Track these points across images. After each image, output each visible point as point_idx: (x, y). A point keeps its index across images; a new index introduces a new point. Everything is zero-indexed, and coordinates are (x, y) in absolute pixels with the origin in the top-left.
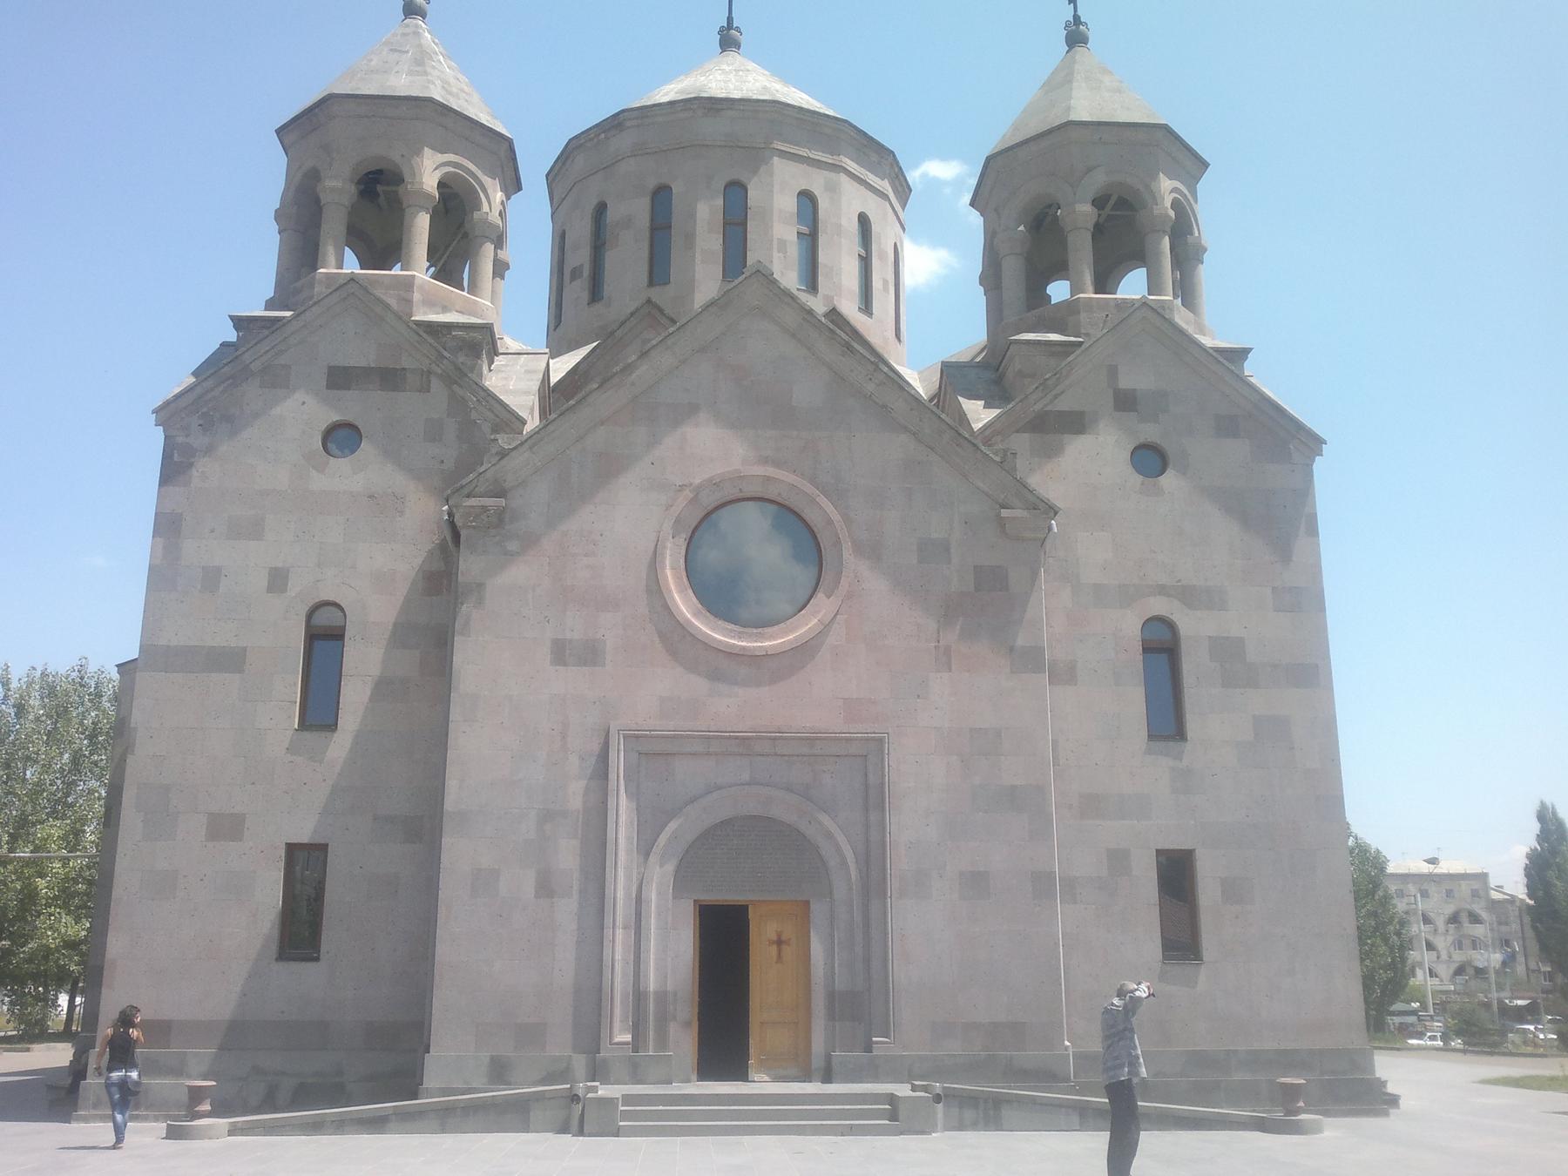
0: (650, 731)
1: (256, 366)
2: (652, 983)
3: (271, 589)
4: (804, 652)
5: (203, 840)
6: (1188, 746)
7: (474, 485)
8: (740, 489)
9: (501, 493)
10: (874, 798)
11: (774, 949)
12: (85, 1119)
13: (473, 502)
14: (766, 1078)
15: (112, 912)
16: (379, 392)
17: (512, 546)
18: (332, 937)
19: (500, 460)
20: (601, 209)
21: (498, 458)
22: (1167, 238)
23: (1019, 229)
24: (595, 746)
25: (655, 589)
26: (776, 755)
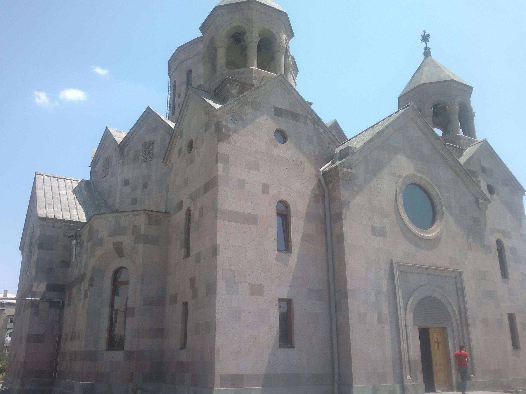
1: (250, 100)
2: (412, 357)
4: (437, 240)
6: (292, 254)
7: (345, 164)
8: (415, 180)
10: (460, 292)
11: (436, 344)
13: (345, 170)
14: (440, 391)
15: (420, 352)
16: (291, 120)
17: (356, 189)
18: (298, 338)
20: (190, 72)
22: (283, 56)
24: (388, 268)
26: (435, 275)
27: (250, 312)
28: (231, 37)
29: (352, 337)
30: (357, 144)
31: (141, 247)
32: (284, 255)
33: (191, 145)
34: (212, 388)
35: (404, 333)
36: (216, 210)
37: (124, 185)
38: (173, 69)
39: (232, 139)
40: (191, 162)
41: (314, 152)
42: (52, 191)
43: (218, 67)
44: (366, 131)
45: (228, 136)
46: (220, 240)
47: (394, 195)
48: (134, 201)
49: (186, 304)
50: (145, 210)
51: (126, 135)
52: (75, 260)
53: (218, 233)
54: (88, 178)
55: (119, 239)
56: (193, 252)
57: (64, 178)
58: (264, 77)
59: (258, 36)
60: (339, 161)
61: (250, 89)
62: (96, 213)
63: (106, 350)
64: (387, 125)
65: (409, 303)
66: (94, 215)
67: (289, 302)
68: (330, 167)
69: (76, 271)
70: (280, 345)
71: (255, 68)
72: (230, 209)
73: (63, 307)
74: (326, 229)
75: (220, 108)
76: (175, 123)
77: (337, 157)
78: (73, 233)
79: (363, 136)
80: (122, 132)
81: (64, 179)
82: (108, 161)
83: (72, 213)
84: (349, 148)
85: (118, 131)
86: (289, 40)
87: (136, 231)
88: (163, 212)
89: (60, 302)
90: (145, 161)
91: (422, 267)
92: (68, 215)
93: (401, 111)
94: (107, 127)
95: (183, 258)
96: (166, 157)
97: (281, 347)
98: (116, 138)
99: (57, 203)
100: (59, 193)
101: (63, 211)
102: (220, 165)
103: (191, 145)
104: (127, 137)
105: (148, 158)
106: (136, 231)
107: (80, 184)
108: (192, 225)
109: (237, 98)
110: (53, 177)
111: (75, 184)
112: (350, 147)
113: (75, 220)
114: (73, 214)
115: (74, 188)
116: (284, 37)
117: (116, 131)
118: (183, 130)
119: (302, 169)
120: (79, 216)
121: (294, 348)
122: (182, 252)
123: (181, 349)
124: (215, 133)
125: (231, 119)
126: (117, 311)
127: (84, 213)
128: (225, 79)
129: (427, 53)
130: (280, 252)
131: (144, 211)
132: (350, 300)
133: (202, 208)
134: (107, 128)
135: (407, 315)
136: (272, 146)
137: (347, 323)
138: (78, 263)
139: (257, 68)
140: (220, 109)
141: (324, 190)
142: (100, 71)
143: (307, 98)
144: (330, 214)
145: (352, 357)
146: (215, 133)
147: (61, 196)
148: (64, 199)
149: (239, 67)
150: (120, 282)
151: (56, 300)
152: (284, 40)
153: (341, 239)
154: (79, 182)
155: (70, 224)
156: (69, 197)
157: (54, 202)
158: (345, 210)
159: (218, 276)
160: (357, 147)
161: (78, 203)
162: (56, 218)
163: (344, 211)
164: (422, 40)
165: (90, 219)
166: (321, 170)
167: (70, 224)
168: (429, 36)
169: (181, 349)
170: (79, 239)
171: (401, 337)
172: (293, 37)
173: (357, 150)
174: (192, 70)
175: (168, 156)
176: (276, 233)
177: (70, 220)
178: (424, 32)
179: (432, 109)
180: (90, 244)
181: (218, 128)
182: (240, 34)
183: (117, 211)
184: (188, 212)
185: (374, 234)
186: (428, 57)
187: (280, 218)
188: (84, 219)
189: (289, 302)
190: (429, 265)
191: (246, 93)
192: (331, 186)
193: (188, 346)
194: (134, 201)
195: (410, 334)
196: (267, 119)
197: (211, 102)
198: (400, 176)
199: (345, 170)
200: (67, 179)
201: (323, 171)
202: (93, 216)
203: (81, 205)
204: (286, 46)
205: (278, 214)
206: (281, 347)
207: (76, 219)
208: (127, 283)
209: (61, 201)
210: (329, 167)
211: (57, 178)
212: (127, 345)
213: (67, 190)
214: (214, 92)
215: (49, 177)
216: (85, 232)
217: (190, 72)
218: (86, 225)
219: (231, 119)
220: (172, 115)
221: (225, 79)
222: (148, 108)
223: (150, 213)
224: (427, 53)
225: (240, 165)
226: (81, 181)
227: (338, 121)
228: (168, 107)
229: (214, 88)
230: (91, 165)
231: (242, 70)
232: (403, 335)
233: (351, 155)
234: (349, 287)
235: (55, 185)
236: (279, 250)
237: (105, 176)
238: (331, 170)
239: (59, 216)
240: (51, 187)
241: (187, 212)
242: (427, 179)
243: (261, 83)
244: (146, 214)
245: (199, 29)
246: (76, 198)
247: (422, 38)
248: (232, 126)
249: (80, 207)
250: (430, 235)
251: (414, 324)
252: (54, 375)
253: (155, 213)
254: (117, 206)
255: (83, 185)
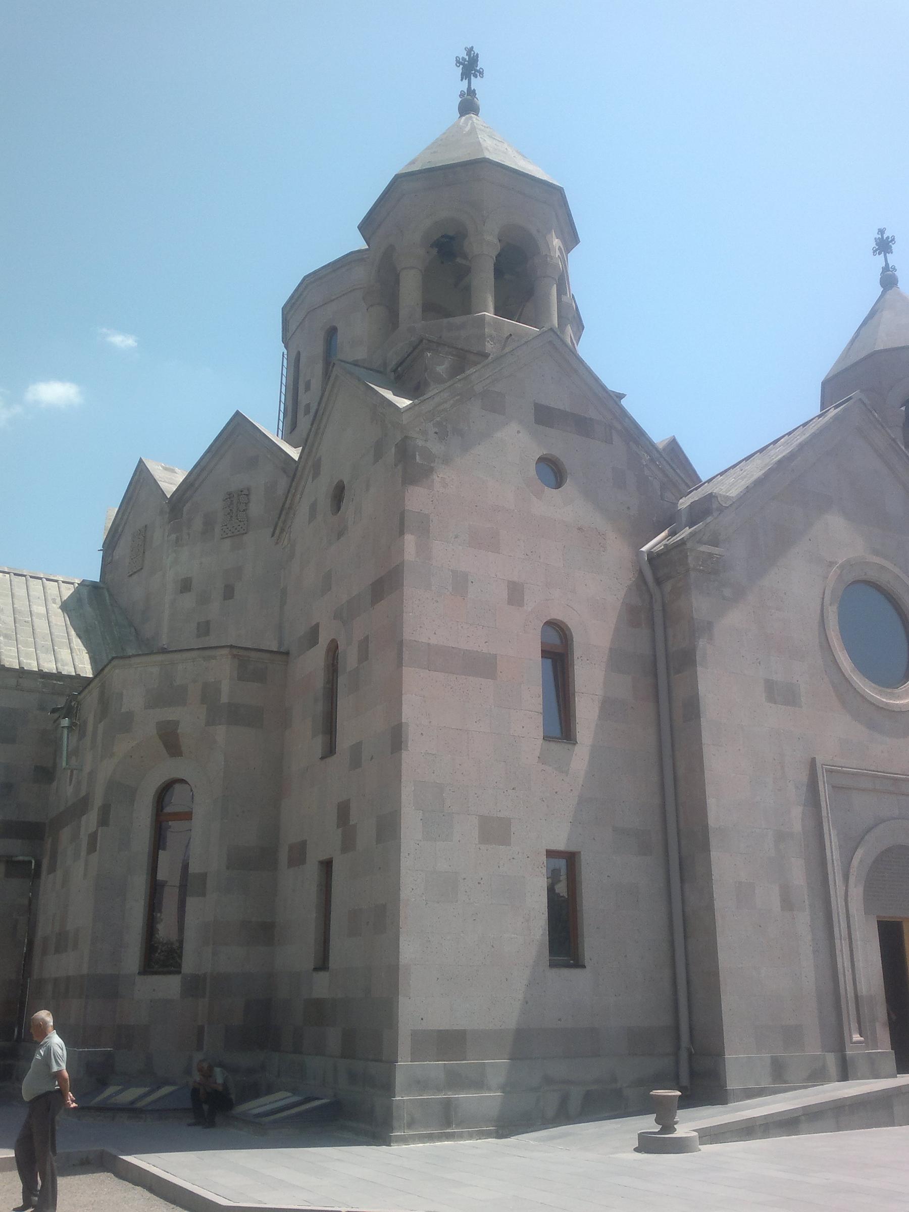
0: (842, 767)
2: (863, 989)
3: (511, 602)
5: (477, 843)
9: (715, 543)
12: (404, 1140)
13: (704, 548)
17: (727, 592)
19: (719, 514)
20: (332, 332)
21: (718, 513)
22: (555, 285)
23: (902, 408)
24: (804, 778)
25: (826, 646)
27: (479, 883)
28: (432, 246)
29: (721, 941)
30: (731, 488)
31: (221, 732)
32: (557, 748)
33: (339, 494)
34: (392, 1062)
35: (844, 932)
36: (401, 643)
37: (181, 592)
38: (293, 327)
39: (436, 478)
40: (340, 535)
41: (628, 508)
42: (13, 607)
43: (403, 313)
44: (747, 459)
45: (427, 472)
46: (409, 713)
47: (819, 608)
48: (204, 629)
49: (327, 865)
50: (232, 647)
51: (184, 477)
52: (67, 764)
53: (404, 697)
54: (95, 576)
55: (170, 714)
56: (344, 742)
57: (42, 577)
58: (511, 335)
59: (496, 241)
60: (687, 528)
61: (479, 363)
62: (114, 655)
63: (139, 973)
64: (800, 444)
65: (855, 862)
66: (113, 658)
67: (571, 859)
68: (668, 543)
69: (70, 790)
70: (550, 960)
71: (490, 314)
72: (434, 641)
73: (37, 874)
74: (656, 686)
75: (408, 408)
76: (301, 448)
77: (684, 519)
78: (61, 702)
79: (742, 470)
80: (177, 470)
81: (41, 579)
82: (143, 535)
83: (59, 656)
84: (711, 497)
85: (166, 469)
86: (568, 250)
87: (209, 694)
88: (271, 652)
89: (32, 862)
90: (229, 535)
91: (884, 777)
92: (50, 661)
93: (833, 413)
94: (141, 458)
95: (320, 757)
96: (280, 524)
97: (553, 965)
98: (162, 485)
99: (25, 634)
100: (30, 611)
101: (38, 652)
102: (410, 541)
103: (339, 494)
104: (188, 481)
105: (236, 529)
106: (209, 694)
107: (77, 592)
108: (342, 680)
109: (448, 384)
110: (15, 574)
111: (67, 592)
112: (714, 494)
113: (66, 673)
114: (62, 659)
115: (63, 600)
116: (556, 243)
117: (161, 468)
118: (320, 459)
119: (602, 549)
120: (77, 664)
121: (584, 967)
122: (318, 744)
123: (316, 969)
124: (396, 465)
125: (436, 433)
126: (163, 884)
127: (86, 657)
128: (421, 341)
129: (888, 280)
130: (549, 741)
131: (229, 649)
132: (715, 855)
133: (367, 639)
134: (141, 461)
135: (849, 890)
136: (531, 494)
137: (710, 908)
138: (75, 772)
139: (495, 315)
140: (409, 408)
141: (652, 598)
142: (122, 341)
143: (612, 384)
144: (666, 650)
145: (722, 988)
146: (396, 465)
147: (34, 618)
148: (41, 625)
149: (448, 315)
150: (169, 814)
151: (21, 858)
152: (557, 250)
153: (692, 709)
154: (77, 585)
155: (55, 682)
156: (53, 619)
157: (17, 632)
158: (702, 643)
159: (403, 797)
160: (731, 495)
161: (73, 633)
162: (23, 668)
163: (701, 645)
164: (876, 250)
165: (103, 670)
166: (644, 549)
167: (55, 682)
168: (893, 240)
169: (316, 969)
170: (76, 716)
171: (837, 942)
172: (577, 244)
173: (729, 503)
174: (337, 328)
175: (285, 522)
176: (539, 696)
177: (55, 671)
178: (881, 231)
179: (903, 408)
180: (101, 726)
181: (405, 452)
182: (451, 238)
183: (164, 651)
184: (333, 649)
185: (771, 699)
186: (891, 288)
187: (549, 662)
188: (87, 671)
189: (571, 859)
190: (899, 773)
191: (468, 372)
192: (668, 586)
193: (333, 963)
194: (204, 629)
195: (857, 935)
196: (518, 432)
197: (388, 395)
198: (831, 564)
199: (704, 548)
200: (48, 580)
201: (650, 553)
202: (110, 661)
203: (80, 638)
204: (560, 263)
205: (545, 654)
206: (553, 965)
207: (68, 670)
208: (187, 816)
209: (35, 627)
210: (664, 542)
211: (24, 576)
212: (189, 965)
213: (48, 603)
214: (393, 371)
215: (8, 575)
216: (91, 700)
217: (332, 332)
218: (92, 685)
219: (436, 433)
220: (291, 430)
221: (421, 341)
222: (238, 414)
223: (242, 653)
224: (888, 280)
225: (456, 538)
226: (79, 582)
227: (676, 438)
228: (282, 415)
229: (393, 364)
230: (103, 547)
231: (458, 320)
232: (841, 936)
233: (715, 514)
234: (712, 822)
235: (21, 592)
236: (546, 738)
237: (135, 573)
238: (668, 550)
239: (30, 664)
240: (12, 599)
241: (329, 650)
242: (896, 570)
243: (503, 349)
244: (234, 656)
245: (357, 229)
246: (68, 623)
247: (876, 244)
248: (436, 447)
249: (77, 643)
250: (902, 702)
251: (867, 912)
252: (18, 1032)
253: (253, 654)
254: (164, 641)
255: (85, 591)
